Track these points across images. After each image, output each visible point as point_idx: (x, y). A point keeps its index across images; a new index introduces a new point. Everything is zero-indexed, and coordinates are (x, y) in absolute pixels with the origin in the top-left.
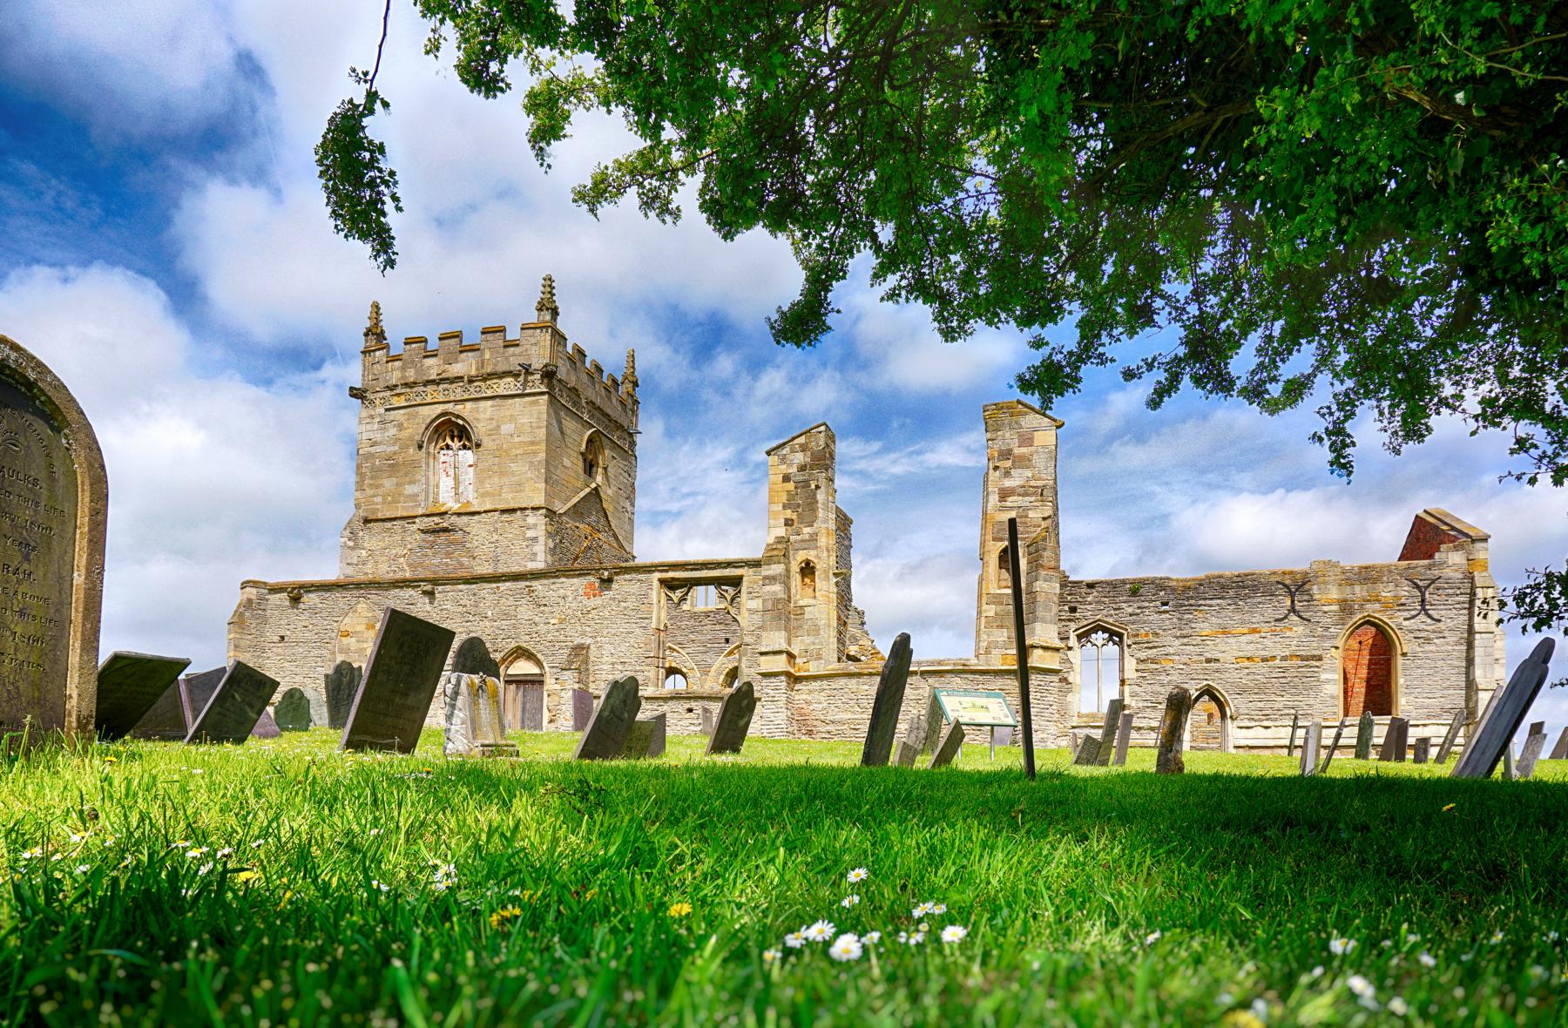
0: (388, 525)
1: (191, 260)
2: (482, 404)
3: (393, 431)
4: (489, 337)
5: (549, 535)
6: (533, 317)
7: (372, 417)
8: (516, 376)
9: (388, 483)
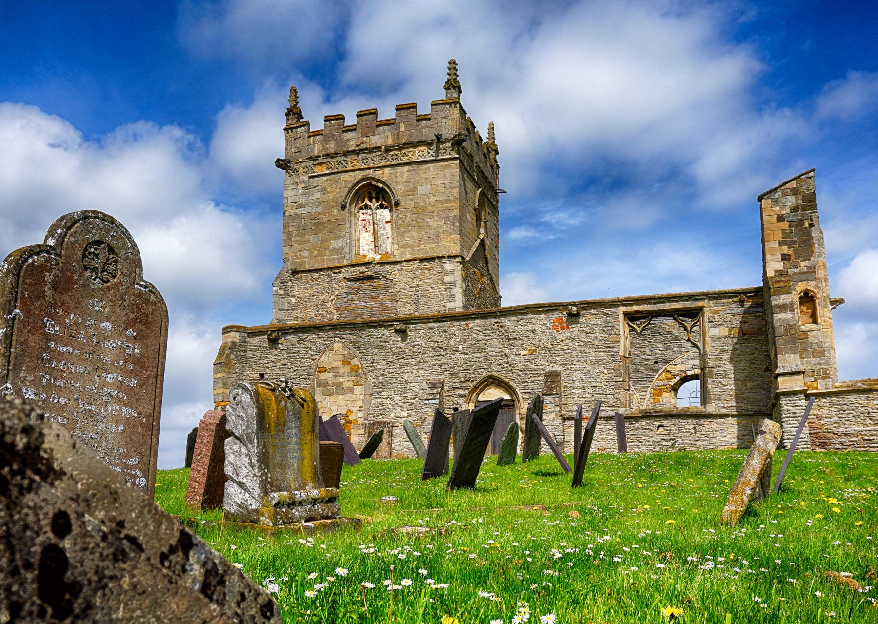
0: (317, 275)
1: (329, 35)
2: (399, 169)
3: (317, 195)
4: (403, 113)
5: (464, 279)
6: (442, 95)
7: (296, 183)
8: (429, 144)
9: (314, 239)
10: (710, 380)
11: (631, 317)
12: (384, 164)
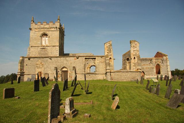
8: (55, 28)
10: (172, 82)
11: (86, 59)
12: (47, 30)
